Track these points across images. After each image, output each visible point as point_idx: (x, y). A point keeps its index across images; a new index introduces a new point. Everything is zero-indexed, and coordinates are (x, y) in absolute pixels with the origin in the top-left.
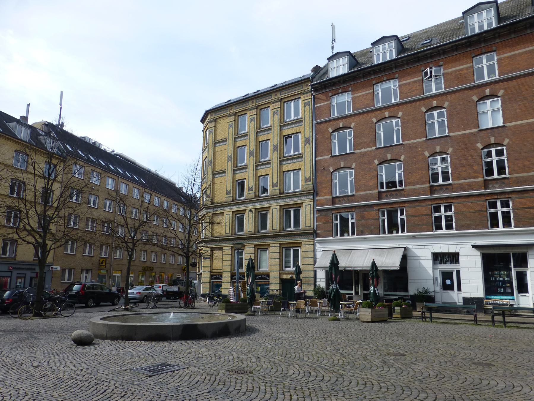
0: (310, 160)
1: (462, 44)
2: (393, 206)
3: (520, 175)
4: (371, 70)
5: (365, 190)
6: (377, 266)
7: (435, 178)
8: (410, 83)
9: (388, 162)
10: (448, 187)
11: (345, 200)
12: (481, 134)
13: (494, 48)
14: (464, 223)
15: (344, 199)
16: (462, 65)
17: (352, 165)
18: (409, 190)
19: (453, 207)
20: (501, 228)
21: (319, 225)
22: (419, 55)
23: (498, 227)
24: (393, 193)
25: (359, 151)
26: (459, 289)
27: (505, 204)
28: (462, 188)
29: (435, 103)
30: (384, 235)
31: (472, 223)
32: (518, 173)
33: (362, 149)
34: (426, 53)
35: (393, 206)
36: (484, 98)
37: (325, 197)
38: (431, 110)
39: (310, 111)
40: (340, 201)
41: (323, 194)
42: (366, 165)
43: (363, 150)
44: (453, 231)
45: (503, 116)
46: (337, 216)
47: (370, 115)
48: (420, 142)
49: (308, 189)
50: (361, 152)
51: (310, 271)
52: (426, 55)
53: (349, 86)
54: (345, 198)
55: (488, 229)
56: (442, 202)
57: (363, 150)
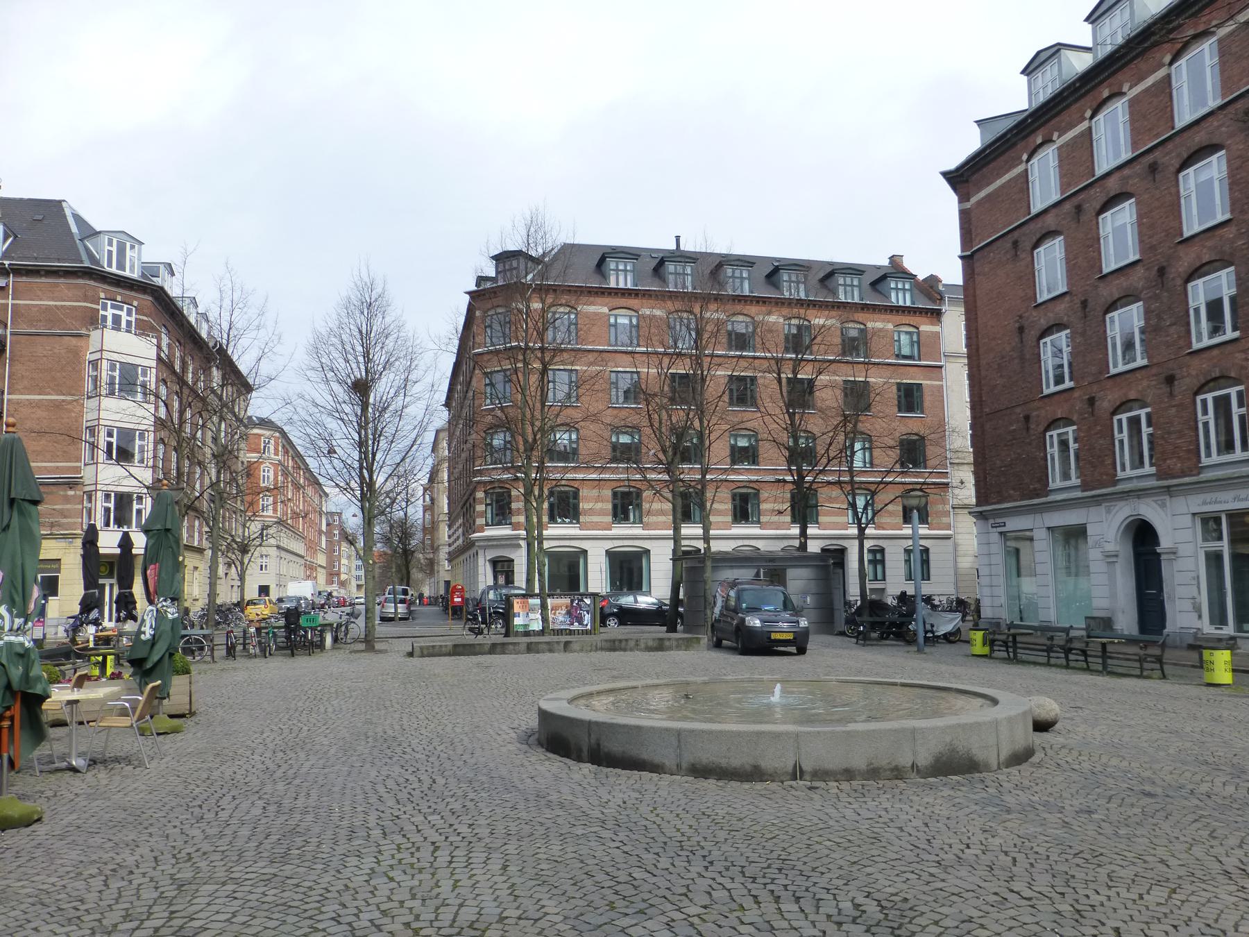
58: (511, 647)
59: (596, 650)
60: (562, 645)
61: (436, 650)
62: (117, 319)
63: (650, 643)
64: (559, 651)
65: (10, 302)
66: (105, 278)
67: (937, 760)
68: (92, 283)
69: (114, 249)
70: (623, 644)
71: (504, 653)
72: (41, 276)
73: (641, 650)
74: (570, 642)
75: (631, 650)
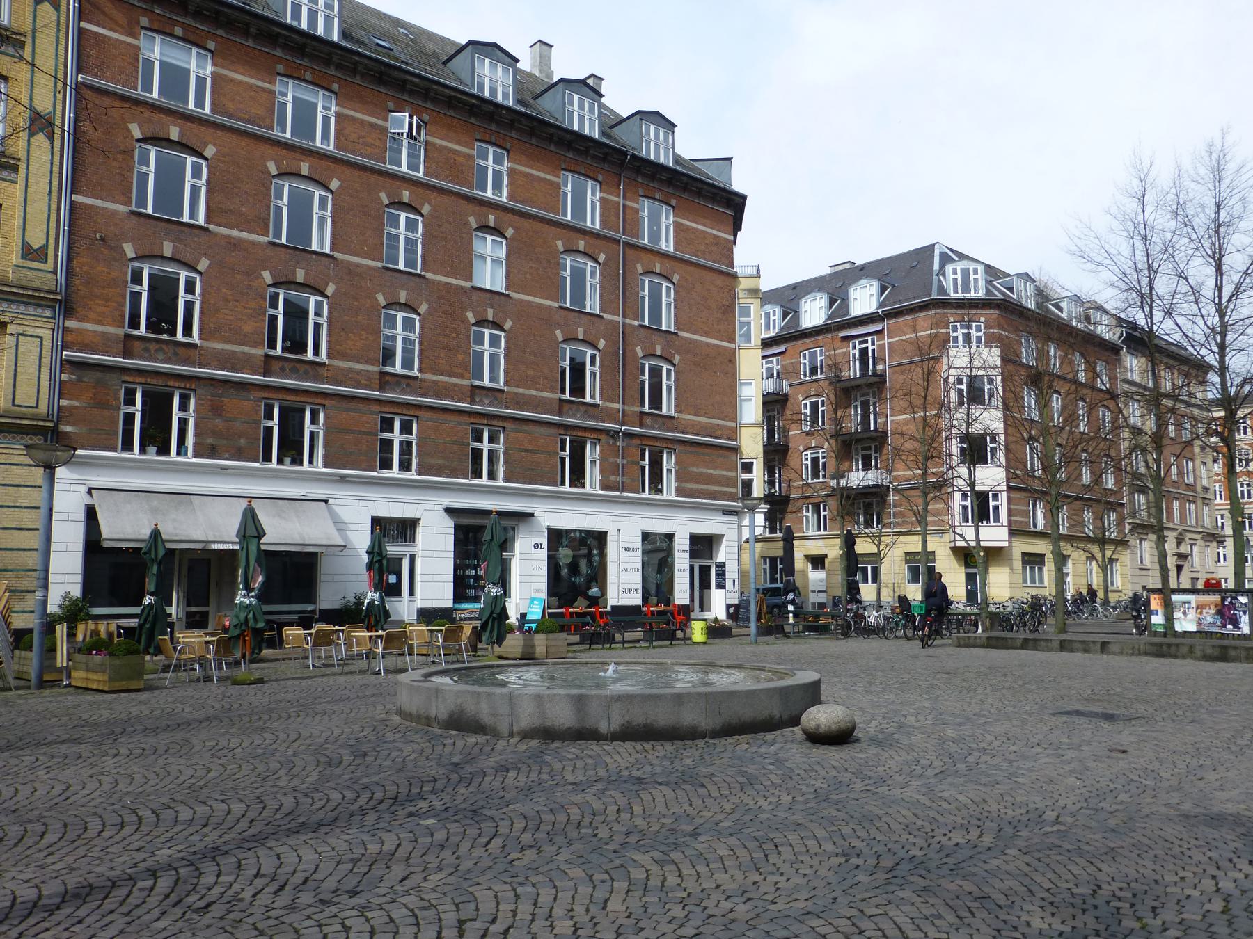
0: (50, 192)
1: (465, 103)
2: (298, 399)
3: (521, 391)
4: (284, 35)
5: (229, 342)
6: (164, 537)
7: (388, 356)
8: (362, 122)
9: (293, 286)
10: (412, 382)
11: (165, 353)
12: (476, 296)
13: (508, 146)
14: (433, 461)
15: (161, 349)
16: (459, 143)
17: (198, 261)
18: (338, 368)
19: (415, 426)
20: (485, 480)
21: (69, 408)
22: (396, 74)
23: (481, 477)
24: (298, 366)
25: (223, 231)
26: (412, 593)
27: (407, 429)
28: (436, 390)
29: (406, 196)
30: (267, 466)
31: (446, 463)
32: (518, 387)
33: (232, 228)
34: (408, 77)
35: (298, 399)
36: (484, 228)
37: (100, 328)
38: (396, 206)
39: (58, 30)
40: (147, 350)
41: (92, 315)
42: (238, 276)
43: (234, 233)
44: (412, 475)
45: (507, 277)
46: (134, 392)
47: (471, 208)
48: (370, 268)
49: (36, 285)
50: (228, 237)
51: (25, 550)
52: (405, 81)
53: (214, 37)
54: (164, 347)
55: (256, 461)
56: (399, 411)
57: (234, 233)
58: (1043, 643)
59: (1140, 654)
60: (1099, 646)
61: (971, 641)
62: (967, 337)
63: (1209, 651)
64: (1096, 652)
65: (886, 341)
66: (946, 304)
67: (451, 715)
68: (940, 311)
69: (959, 276)
70: (1173, 649)
71: (1036, 649)
72: (905, 315)
73: (1196, 659)
74: (1108, 643)
75: (1184, 657)
